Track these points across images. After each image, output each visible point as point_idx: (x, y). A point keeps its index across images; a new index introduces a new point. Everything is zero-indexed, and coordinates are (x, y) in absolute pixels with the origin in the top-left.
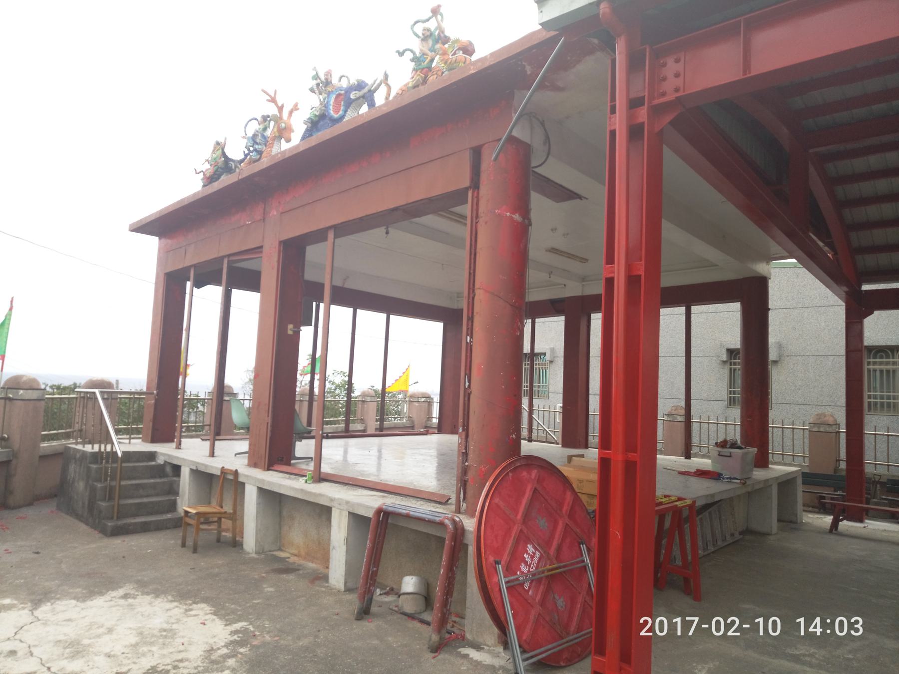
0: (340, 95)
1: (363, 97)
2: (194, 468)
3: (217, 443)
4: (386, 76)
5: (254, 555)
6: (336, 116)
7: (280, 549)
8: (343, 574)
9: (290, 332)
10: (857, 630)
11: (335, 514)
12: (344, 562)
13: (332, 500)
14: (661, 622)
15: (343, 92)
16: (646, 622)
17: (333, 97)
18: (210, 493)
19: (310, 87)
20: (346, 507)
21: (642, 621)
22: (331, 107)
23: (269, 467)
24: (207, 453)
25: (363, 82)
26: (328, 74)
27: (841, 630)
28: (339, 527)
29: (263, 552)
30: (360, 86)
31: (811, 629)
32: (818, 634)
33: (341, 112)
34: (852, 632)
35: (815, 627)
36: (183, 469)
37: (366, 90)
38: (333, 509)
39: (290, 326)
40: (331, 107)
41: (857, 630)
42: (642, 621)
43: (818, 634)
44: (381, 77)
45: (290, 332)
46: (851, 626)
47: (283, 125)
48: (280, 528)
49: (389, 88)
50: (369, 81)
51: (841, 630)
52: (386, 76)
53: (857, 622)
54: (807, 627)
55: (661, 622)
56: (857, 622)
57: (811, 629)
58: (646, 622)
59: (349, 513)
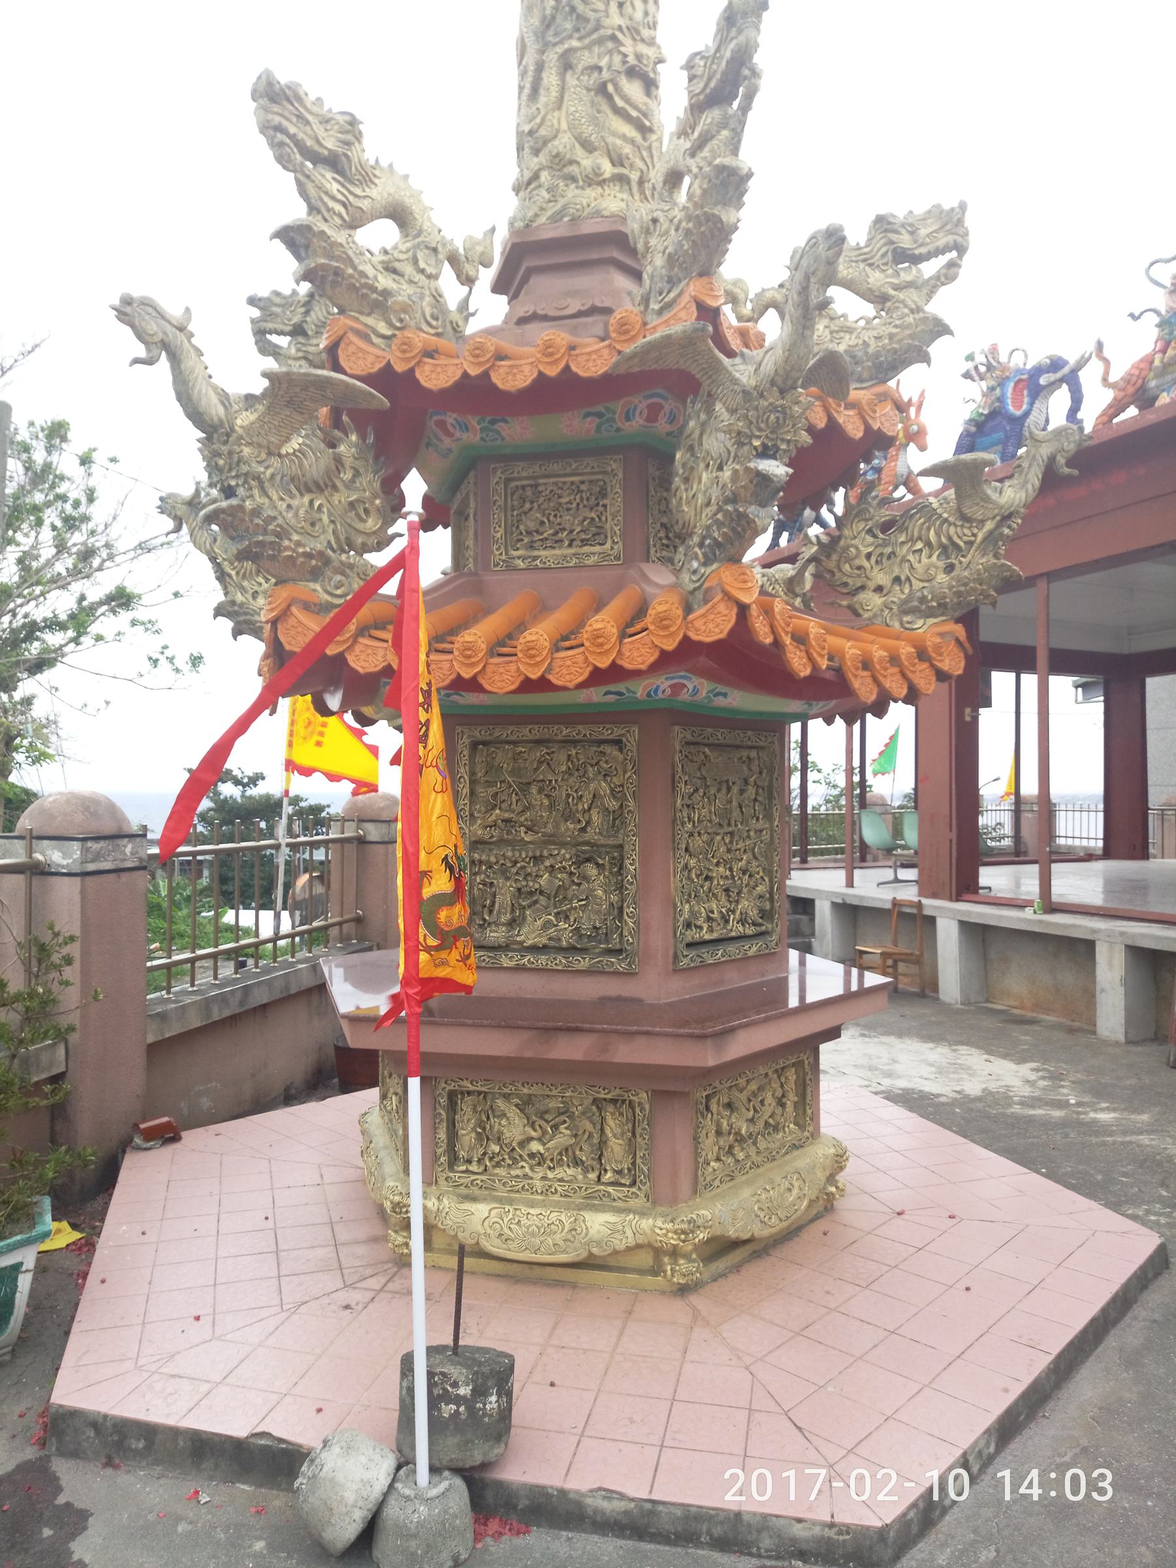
0: (1020, 381)
1: (1062, 380)
2: (839, 901)
3: (857, 872)
4: (1100, 346)
5: (959, 1006)
6: (1018, 413)
7: (987, 1001)
8: (1123, 1021)
9: (968, 719)
10: (1102, 1492)
11: (1101, 951)
12: (1123, 1007)
13: (1094, 931)
14: (761, 1477)
15: (1025, 377)
16: (735, 1477)
17: (1010, 386)
18: (855, 935)
19: (964, 371)
20: (1119, 939)
21: (727, 1476)
22: (1009, 401)
23: (958, 899)
24: (844, 883)
25: (1060, 358)
26: (994, 350)
27: (1075, 1492)
28: (1110, 964)
29: (969, 1004)
30: (1056, 364)
31: (1022, 1490)
32: (1036, 1498)
33: (1025, 407)
34: (1095, 1495)
35: (1030, 1486)
36: (818, 904)
37: (1066, 370)
38: (1098, 943)
39: (968, 711)
40: (1009, 401)
41: (1102, 1492)
42: (727, 1476)
43: (1036, 1498)
44: (1091, 347)
45: (968, 719)
46: (1093, 1485)
47: (915, 428)
48: (986, 976)
49: (1107, 363)
50: (1072, 359)
51: (1075, 1492)
52: (1100, 346)
53: (1103, 1477)
54: (1015, 1487)
55: (761, 1477)
56: (1103, 1477)
57: (1022, 1490)
58: (735, 1477)
59: (1126, 946)
